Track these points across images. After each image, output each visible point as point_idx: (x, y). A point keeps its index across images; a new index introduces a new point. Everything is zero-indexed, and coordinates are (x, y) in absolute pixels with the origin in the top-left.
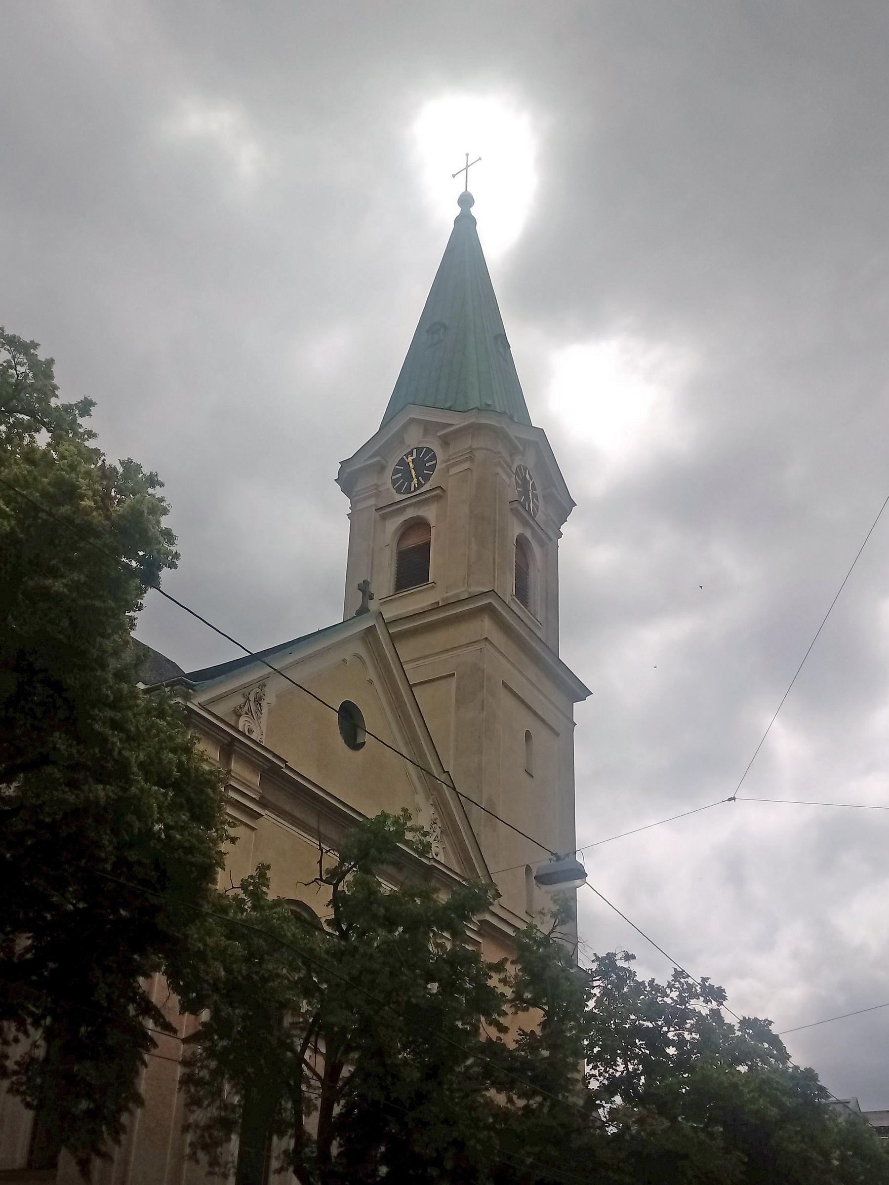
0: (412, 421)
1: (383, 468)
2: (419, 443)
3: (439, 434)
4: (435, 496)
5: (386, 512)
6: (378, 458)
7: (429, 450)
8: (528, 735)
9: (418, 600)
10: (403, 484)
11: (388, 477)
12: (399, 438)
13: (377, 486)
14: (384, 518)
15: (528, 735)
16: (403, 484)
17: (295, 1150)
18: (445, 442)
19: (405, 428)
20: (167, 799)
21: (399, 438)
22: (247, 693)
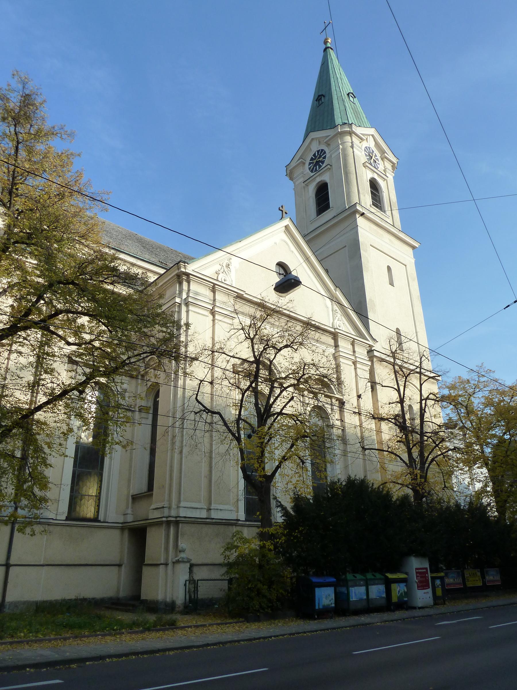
0: (313, 139)
1: (304, 164)
2: (378, 375)
3: (325, 141)
4: (327, 169)
5: (307, 182)
6: (301, 160)
7: (322, 150)
8: (389, 268)
9: (327, 215)
10: (313, 168)
11: (307, 166)
12: (308, 147)
13: (302, 173)
14: (307, 185)
15: (389, 268)
16: (313, 168)
17: (115, 269)
18: (328, 145)
19: (310, 143)
20: (111, 262)
21: (308, 147)
22: (221, 263)
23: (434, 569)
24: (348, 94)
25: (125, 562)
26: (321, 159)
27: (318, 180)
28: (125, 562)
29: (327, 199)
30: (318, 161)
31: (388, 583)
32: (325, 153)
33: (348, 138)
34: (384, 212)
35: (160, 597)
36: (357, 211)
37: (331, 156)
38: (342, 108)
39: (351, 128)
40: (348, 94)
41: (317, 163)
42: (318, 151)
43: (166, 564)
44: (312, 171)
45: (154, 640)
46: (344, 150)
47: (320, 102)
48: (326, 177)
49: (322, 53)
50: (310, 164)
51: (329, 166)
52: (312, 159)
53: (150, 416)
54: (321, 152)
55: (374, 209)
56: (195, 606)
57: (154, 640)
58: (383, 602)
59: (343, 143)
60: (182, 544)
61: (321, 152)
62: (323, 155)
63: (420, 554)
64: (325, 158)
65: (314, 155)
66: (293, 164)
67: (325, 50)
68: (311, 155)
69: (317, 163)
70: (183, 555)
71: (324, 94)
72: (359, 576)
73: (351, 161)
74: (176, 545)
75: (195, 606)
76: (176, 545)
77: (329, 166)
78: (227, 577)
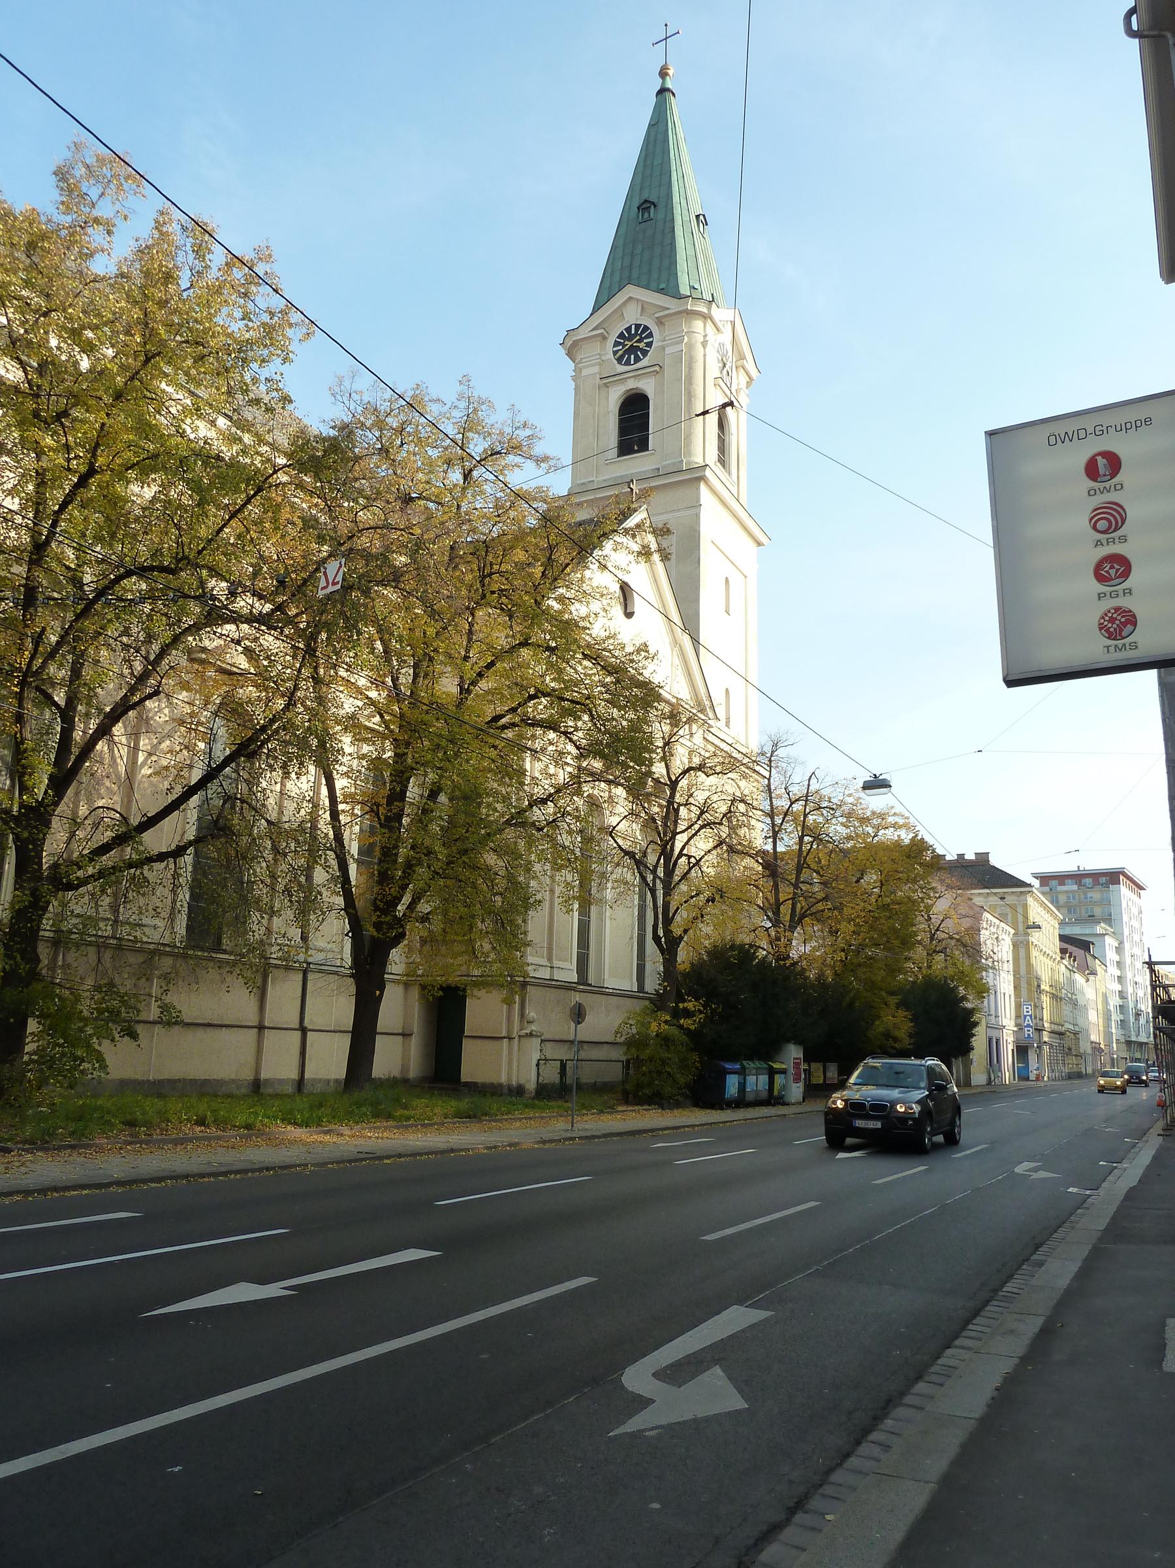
0: (630, 298)
5: (607, 381)
7: (646, 328)
18: (660, 322)
23: (808, 1058)
24: (698, 217)
25: (415, 1030)
26: (642, 345)
27: (632, 384)
28: (415, 1030)
29: (645, 426)
30: (633, 345)
31: (772, 1073)
32: (651, 335)
33: (698, 325)
34: (729, 474)
35: (504, 1080)
36: (703, 478)
37: (663, 348)
38: (691, 252)
39: (709, 309)
40: (698, 217)
41: (633, 350)
42: (638, 326)
43: (510, 1039)
44: (619, 360)
45: (471, 1138)
46: (690, 346)
47: (646, 215)
48: (647, 386)
49: (653, 100)
50: (616, 344)
51: (657, 368)
52: (621, 336)
53: (338, 793)
54: (643, 332)
55: (718, 469)
56: (556, 1092)
57: (471, 1138)
58: (764, 1095)
59: (690, 333)
60: (531, 1013)
61: (643, 332)
62: (646, 337)
63: (798, 1042)
64: (649, 345)
65: (628, 329)
66: (584, 333)
67: (663, 91)
68: (621, 328)
69: (633, 350)
70: (533, 1027)
71: (653, 198)
72: (758, 1064)
73: (699, 373)
74: (522, 1015)
75: (556, 1092)
76: (522, 1015)
77: (657, 368)
78: (624, 1058)
